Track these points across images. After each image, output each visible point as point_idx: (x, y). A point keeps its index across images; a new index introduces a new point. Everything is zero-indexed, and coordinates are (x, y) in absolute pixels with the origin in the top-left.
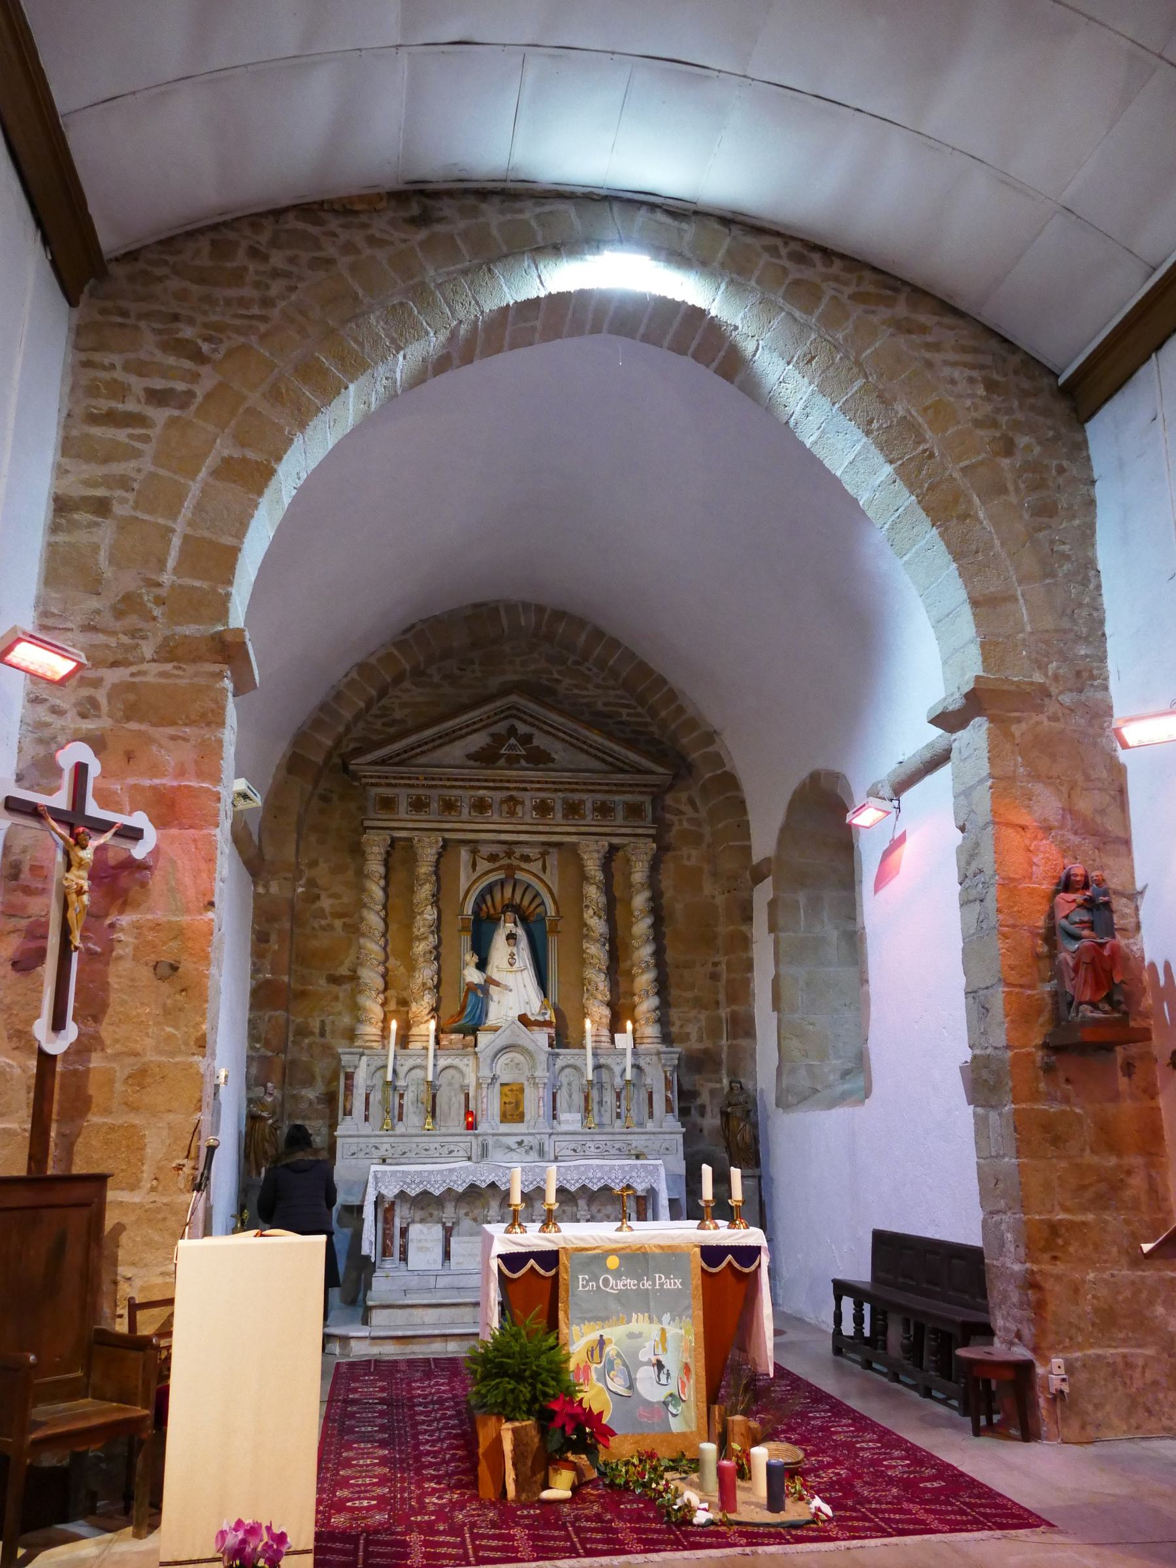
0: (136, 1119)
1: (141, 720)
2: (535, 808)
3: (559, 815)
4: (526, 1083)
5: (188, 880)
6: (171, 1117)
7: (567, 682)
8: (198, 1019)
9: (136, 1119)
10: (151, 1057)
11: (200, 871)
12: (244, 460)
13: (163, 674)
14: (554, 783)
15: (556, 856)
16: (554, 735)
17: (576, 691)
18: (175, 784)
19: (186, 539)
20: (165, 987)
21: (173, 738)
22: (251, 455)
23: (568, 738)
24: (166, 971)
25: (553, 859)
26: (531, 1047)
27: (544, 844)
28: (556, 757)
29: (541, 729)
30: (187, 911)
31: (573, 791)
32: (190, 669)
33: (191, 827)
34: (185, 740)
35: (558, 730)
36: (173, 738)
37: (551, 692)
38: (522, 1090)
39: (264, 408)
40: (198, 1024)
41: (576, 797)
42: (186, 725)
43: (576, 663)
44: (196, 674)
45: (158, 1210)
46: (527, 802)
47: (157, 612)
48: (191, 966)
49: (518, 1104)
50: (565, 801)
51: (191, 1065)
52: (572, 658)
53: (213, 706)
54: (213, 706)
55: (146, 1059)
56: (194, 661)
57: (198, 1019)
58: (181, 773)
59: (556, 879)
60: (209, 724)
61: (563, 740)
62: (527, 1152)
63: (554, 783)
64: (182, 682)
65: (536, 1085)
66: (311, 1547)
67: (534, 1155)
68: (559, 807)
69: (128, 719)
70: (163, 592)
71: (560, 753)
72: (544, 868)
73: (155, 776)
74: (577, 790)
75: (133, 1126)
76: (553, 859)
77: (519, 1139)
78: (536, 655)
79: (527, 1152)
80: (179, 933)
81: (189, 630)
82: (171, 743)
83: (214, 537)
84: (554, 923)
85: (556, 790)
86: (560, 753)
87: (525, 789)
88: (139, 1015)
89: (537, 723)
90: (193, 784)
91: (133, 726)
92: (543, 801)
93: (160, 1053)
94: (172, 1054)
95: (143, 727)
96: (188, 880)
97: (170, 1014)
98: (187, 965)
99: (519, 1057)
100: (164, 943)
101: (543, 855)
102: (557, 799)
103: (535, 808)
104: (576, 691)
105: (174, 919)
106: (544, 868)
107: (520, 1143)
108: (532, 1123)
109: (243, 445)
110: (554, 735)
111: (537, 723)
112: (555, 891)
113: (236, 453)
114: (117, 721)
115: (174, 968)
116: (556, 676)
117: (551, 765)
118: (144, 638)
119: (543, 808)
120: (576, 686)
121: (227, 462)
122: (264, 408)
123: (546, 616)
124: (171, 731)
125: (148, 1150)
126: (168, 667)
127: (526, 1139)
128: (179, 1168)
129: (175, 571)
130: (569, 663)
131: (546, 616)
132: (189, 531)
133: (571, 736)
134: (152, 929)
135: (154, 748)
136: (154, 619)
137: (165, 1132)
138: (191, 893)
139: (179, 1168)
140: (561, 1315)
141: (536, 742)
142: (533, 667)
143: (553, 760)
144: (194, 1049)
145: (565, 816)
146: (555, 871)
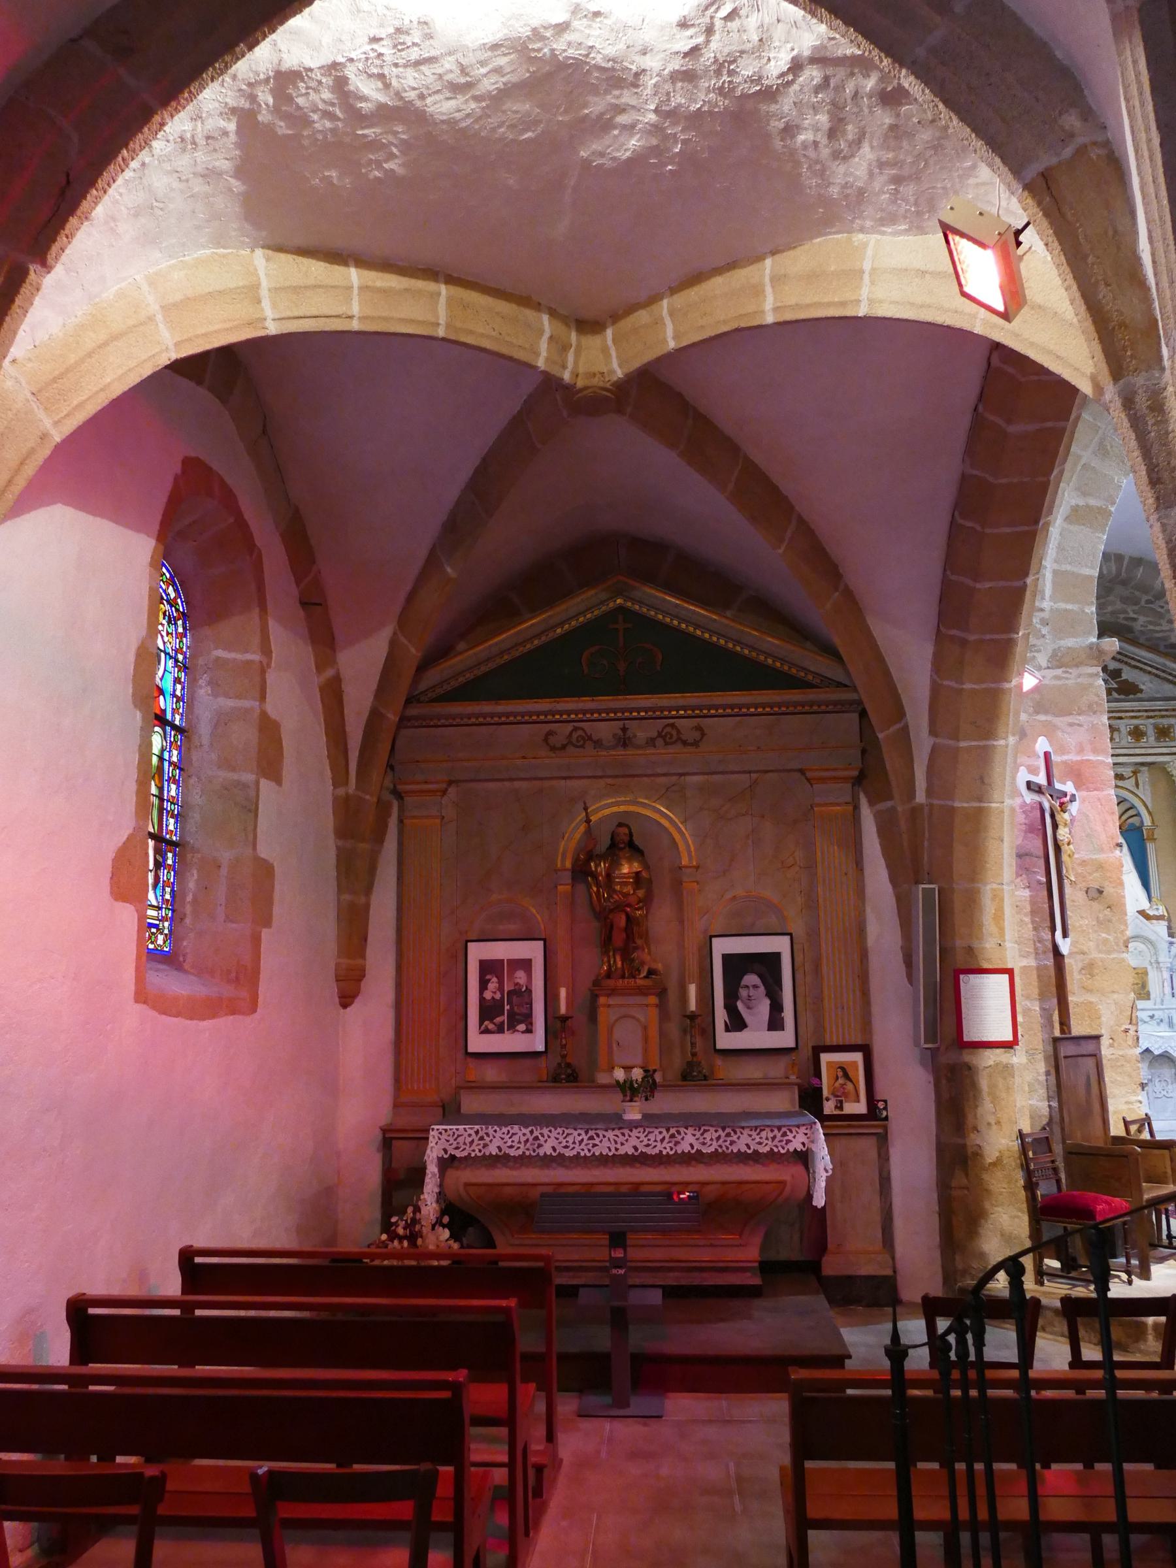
0: (1093, 998)
1: (1046, 712)
2: (1130, 733)
3: (1152, 739)
4: (1149, 968)
5: (1099, 828)
6: (1115, 996)
7: (1142, 619)
8: (1122, 927)
9: (1093, 998)
10: (1094, 955)
11: (1106, 822)
12: (1087, 506)
13: (1057, 678)
14: (1146, 711)
15: (1147, 774)
16: (1141, 669)
17: (1151, 627)
18: (1079, 758)
19: (1055, 573)
20: (1095, 904)
21: (1071, 725)
22: (1092, 502)
23: (1154, 671)
24: (1096, 895)
25: (1144, 776)
26: (1153, 937)
27: (1137, 764)
28: (1142, 687)
29: (1126, 663)
30: (1102, 850)
31: (1163, 717)
32: (1074, 672)
33: (1095, 789)
34: (1079, 725)
35: (1146, 664)
36: (1071, 725)
37: (1130, 630)
38: (1146, 973)
39: (1095, 463)
40: (1122, 932)
41: (1165, 722)
42: (1079, 714)
43: (1148, 602)
44: (1079, 676)
45: (1117, 1060)
46: (1123, 729)
47: (1044, 631)
48: (1111, 890)
49: (1144, 985)
50: (1156, 726)
51: (1123, 960)
52: (1145, 598)
53: (1096, 699)
54: (1096, 699)
55: (1092, 956)
56: (1077, 666)
57: (1122, 927)
58: (1081, 750)
59: (1149, 793)
60: (1095, 713)
61: (1150, 673)
62: (1158, 1024)
63: (1146, 711)
64: (1069, 682)
65: (1159, 968)
66: (926, 1340)
67: (1164, 1026)
68: (1151, 731)
69: (1037, 713)
70: (1046, 615)
71: (1147, 684)
72: (1137, 785)
73: (1063, 754)
74: (1168, 716)
75: (1091, 1003)
76: (1144, 776)
77: (1150, 1013)
78: (1111, 598)
79: (1158, 1024)
80: (1100, 867)
81: (1070, 642)
82: (1069, 729)
83: (1075, 570)
84: (1151, 831)
85: (1148, 717)
86: (1147, 684)
87: (1120, 718)
88: (1081, 926)
89: (1125, 659)
90: (1092, 757)
91: (1042, 717)
92: (1137, 727)
93: (1100, 952)
94: (1109, 952)
95: (1049, 718)
96: (1099, 828)
97: (1103, 924)
98: (1109, 890)
99: (1141, 947)
100: (1090, 874)
101: (1135, 773)
102: (1148, 726)
103: (1130, 733)
104: (1151, 627)
105: (1094, 857)
106: (1137, 785)
107: (1152, 1017)
108: (1159, 1000)
109: (1085, 494)
110: (1141, 669)
111: (1125, 659)
112: (1149, 805)
113: (1081, 502)
114: (1030, 715)
115: (1101, 892)
116: (1132, 615)
117: (1139, 695)
118: (1039, 651)
119: (1137, 733)
120: (1151, 623)
121: (1075, 509)
122: (1095, 463)
123: (1125, 562)
124: (1070, 719)
125: (1103, 1019)
126: (1059, 672)
127: (1158, 1014)
128: (1126, 1031)
129: (1052, 598)
130: (1143, 603)
131: (1125, 562)
132: (1056, 566)
133: (1157, 669)
134: (1080, 864)
135: (1060, 734)
136: (1043, 636)
137: (1113, 1007)
138: (1103, 837)
139: (1126, 1031)
140: (571, 1189)
141: (1124, 676)
142: (1110, 609)
143: (1141, 691)
144: (1124, 949)
145: (1158, 739)
146: (1147, 787)
